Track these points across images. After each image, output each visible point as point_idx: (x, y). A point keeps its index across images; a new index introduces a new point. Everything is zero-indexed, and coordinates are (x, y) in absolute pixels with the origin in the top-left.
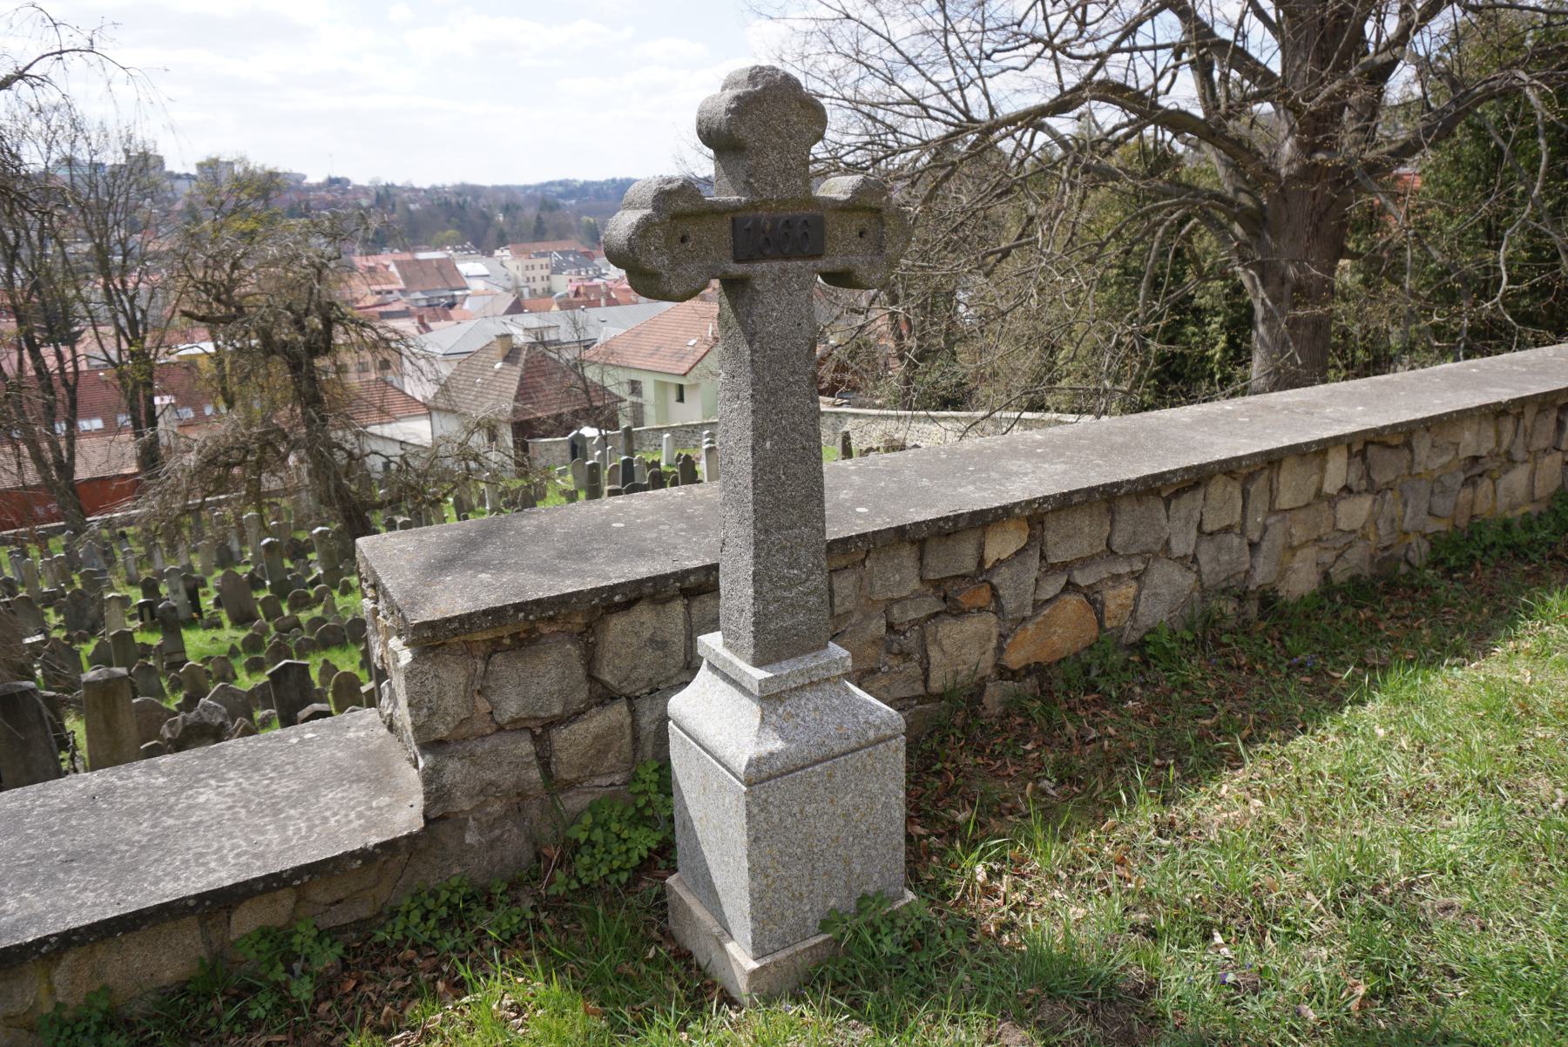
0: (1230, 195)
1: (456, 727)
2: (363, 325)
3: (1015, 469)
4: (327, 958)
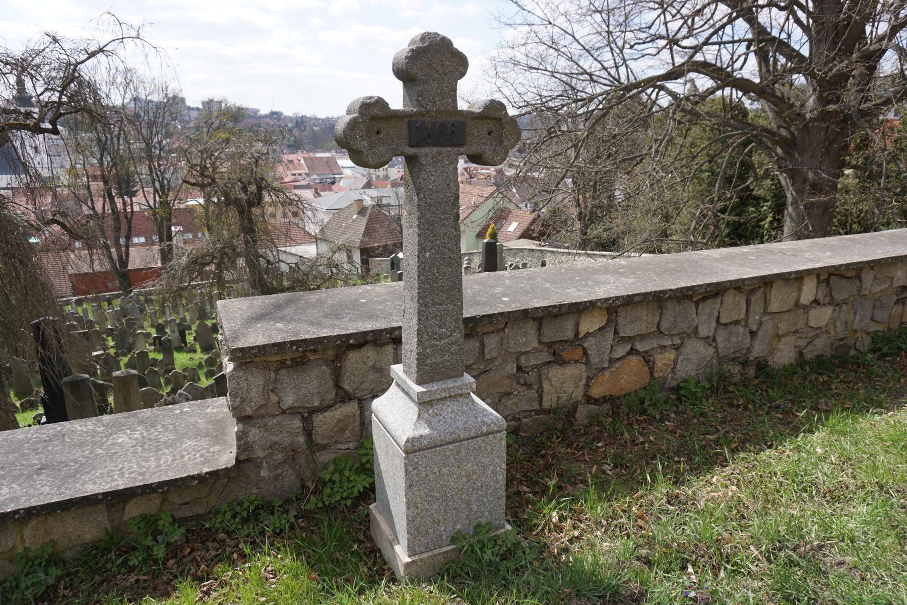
0: (775, 129)
3: (603, 280)
4: (177, 535)
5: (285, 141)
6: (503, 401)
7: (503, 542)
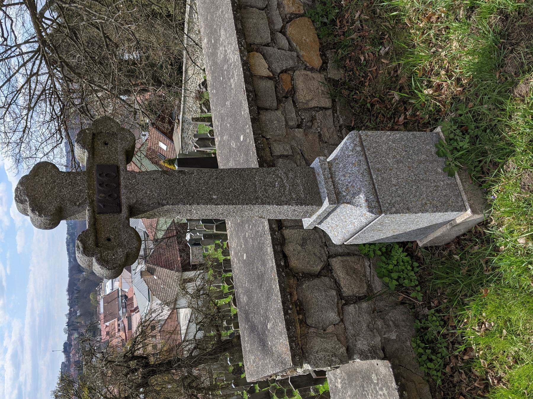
1: (341, 343)
2: (135, 342)
3: (222, 56)
5: (91, 338)
6: (326, 140)
7: (452, 132)
